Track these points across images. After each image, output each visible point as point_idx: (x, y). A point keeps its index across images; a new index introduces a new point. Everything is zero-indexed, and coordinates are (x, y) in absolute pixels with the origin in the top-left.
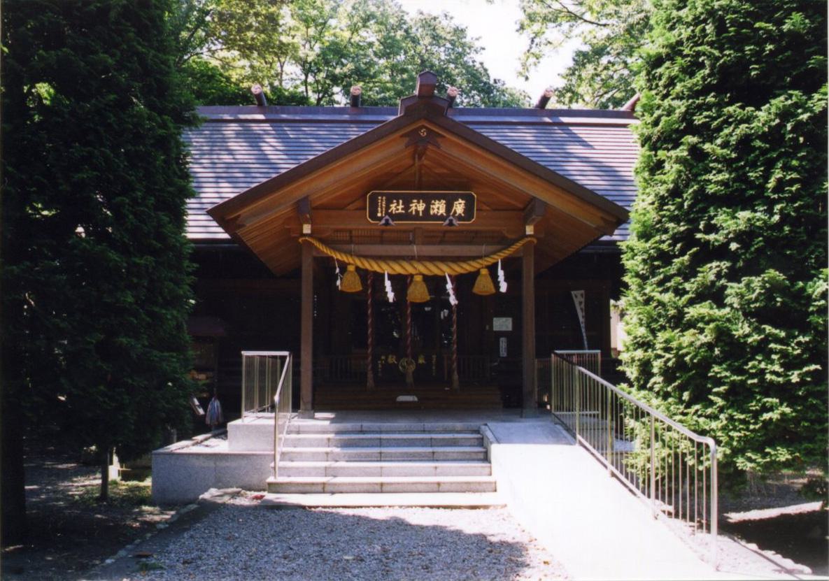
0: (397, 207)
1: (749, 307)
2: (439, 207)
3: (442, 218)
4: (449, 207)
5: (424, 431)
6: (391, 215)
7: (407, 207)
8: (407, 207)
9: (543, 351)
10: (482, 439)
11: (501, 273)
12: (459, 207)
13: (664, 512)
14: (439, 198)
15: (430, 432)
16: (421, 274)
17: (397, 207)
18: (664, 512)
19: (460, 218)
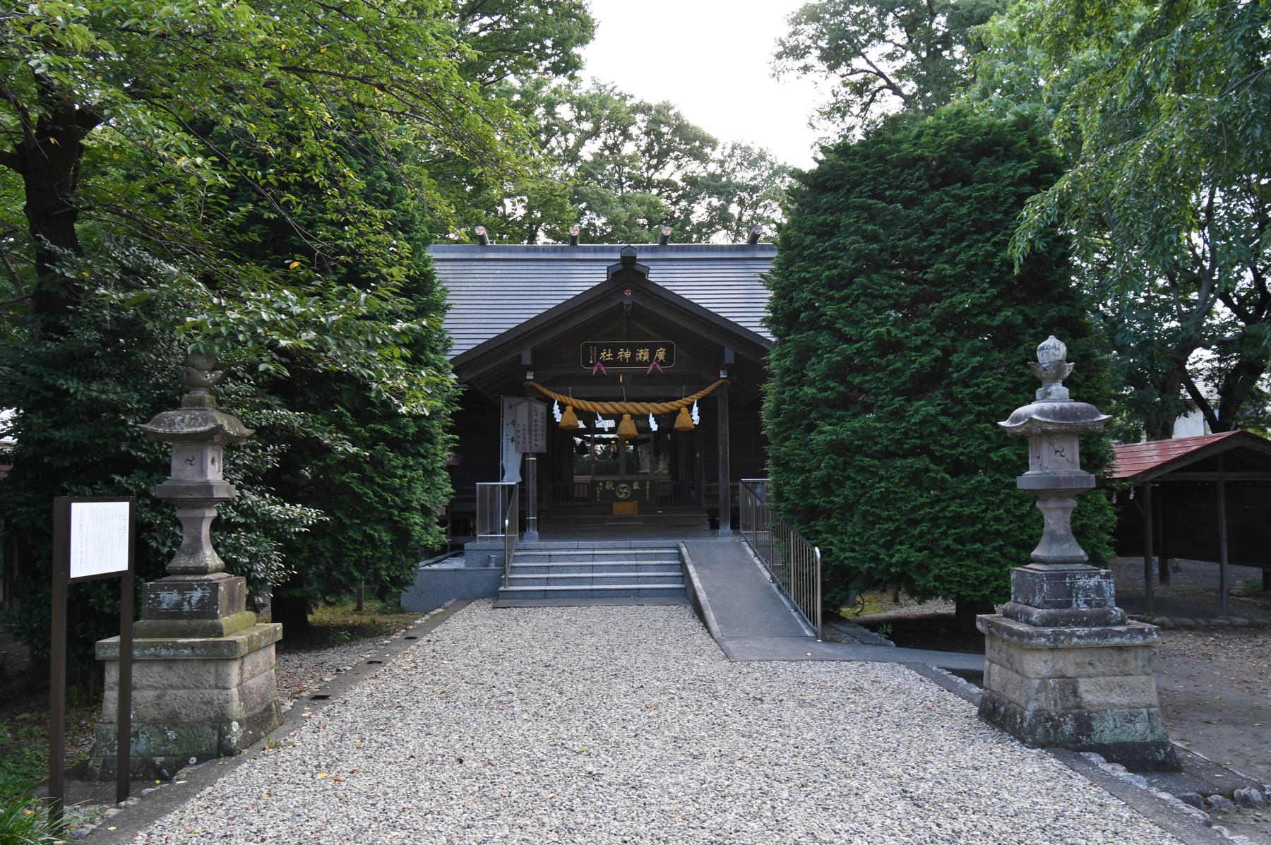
0: (606, 355)
1: (1149, 323)
2: (643, 355)
3: (646, 363)
4: (652, 354)
5: (630, 548)
6: (601, 361)
7: (615, 355)
8: (615, 355)
9: (735, 477)
10: (230, 753)
11: (695, 409)
12: (661, 354)
13: (632, 97)
14: (643, 346)
15: (636, 548)
16: (629, 413)
17: (606, 355)
18: (632, 97)
19: (661, 363)
